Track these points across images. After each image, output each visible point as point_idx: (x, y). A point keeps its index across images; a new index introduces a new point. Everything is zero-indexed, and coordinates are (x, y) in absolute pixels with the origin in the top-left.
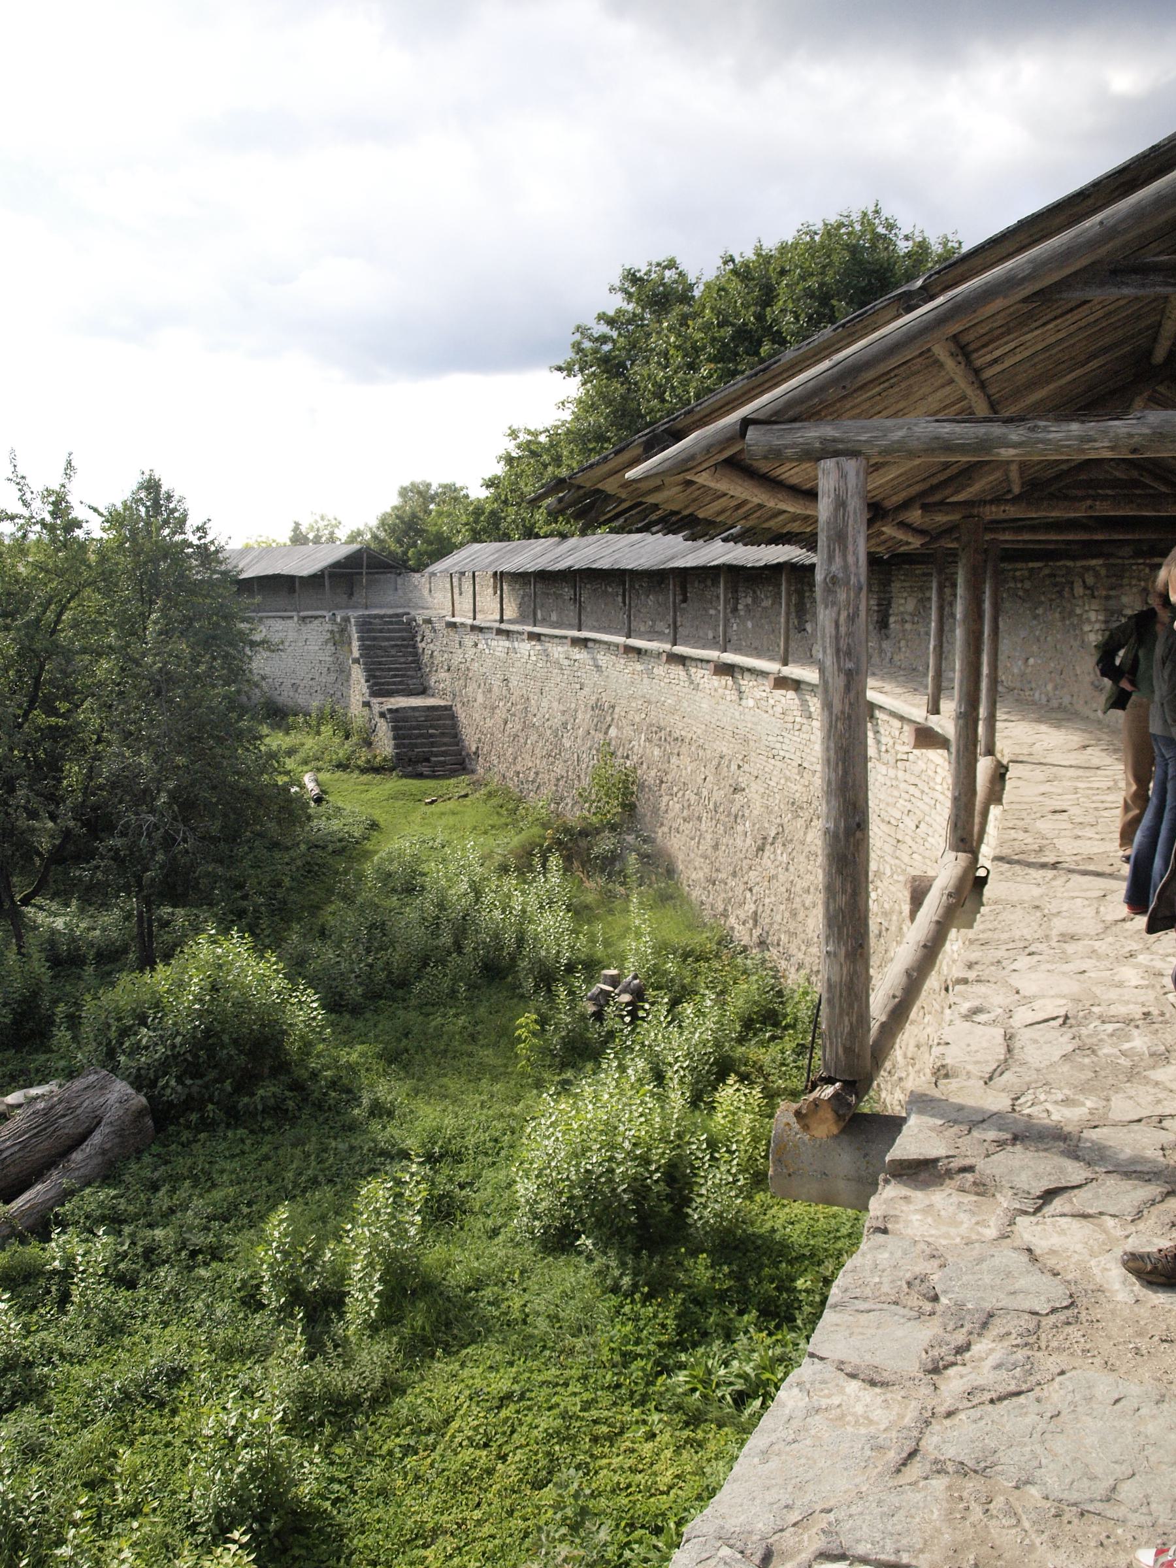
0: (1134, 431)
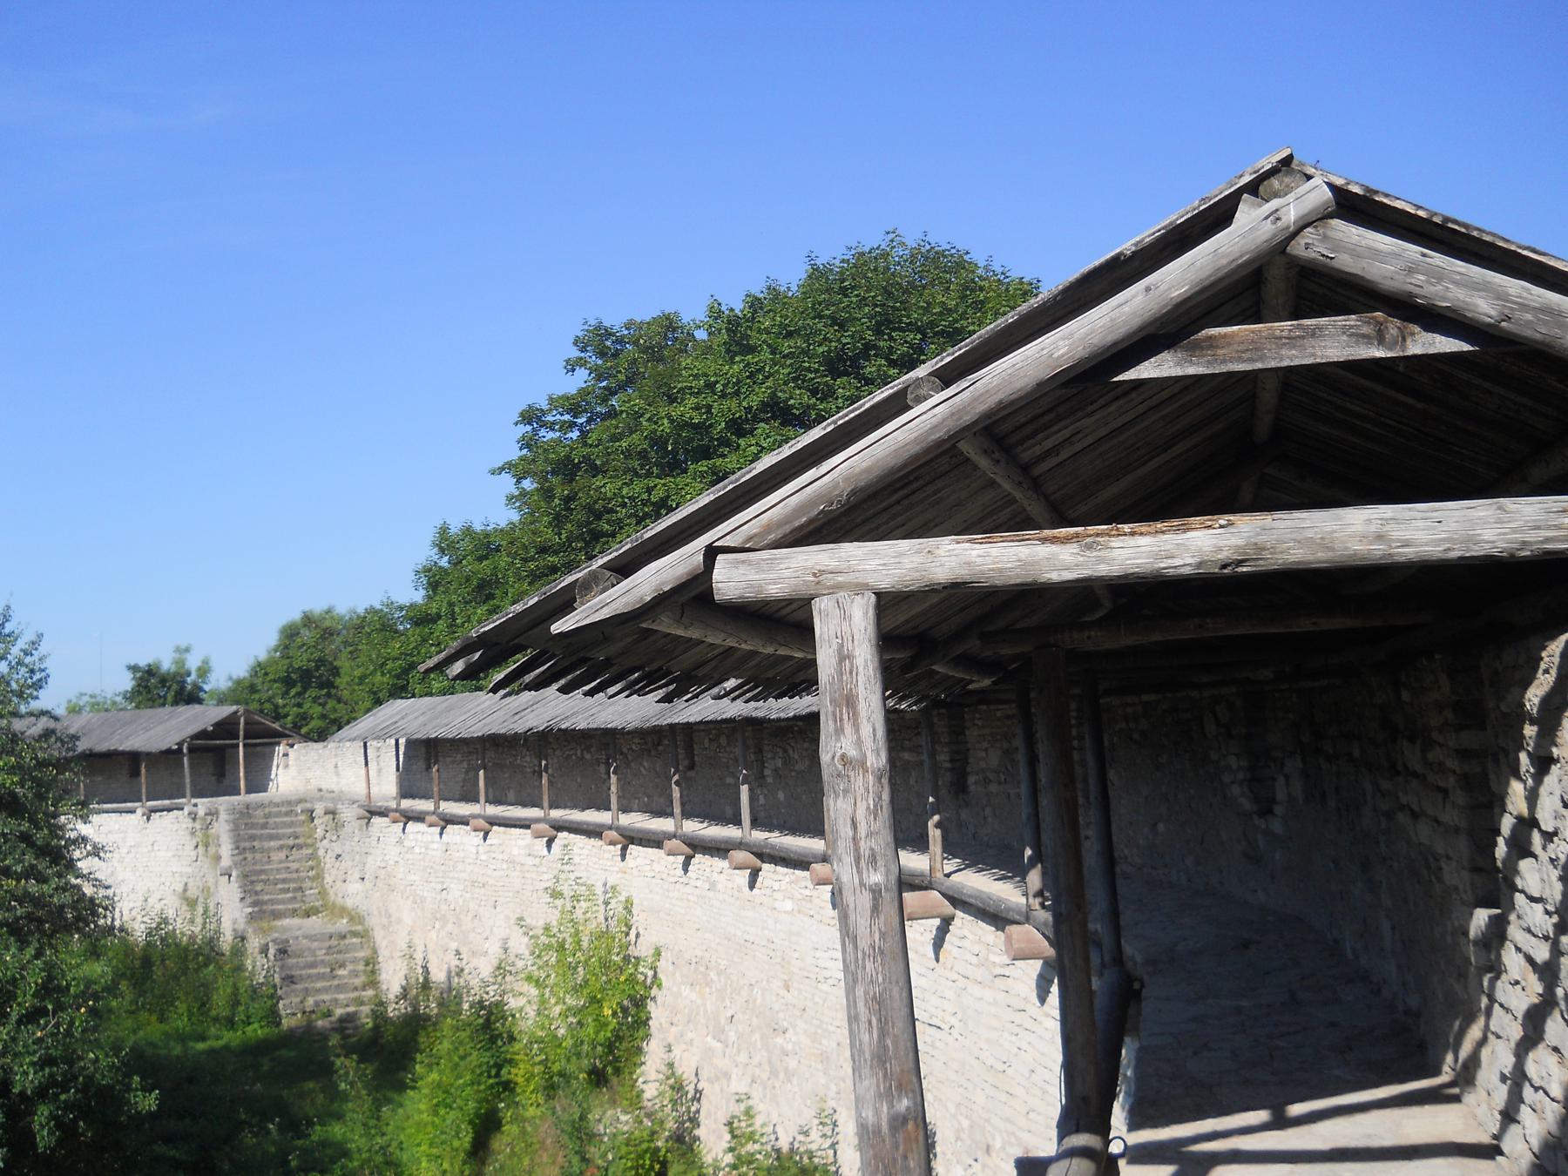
0: (1222, 543)
